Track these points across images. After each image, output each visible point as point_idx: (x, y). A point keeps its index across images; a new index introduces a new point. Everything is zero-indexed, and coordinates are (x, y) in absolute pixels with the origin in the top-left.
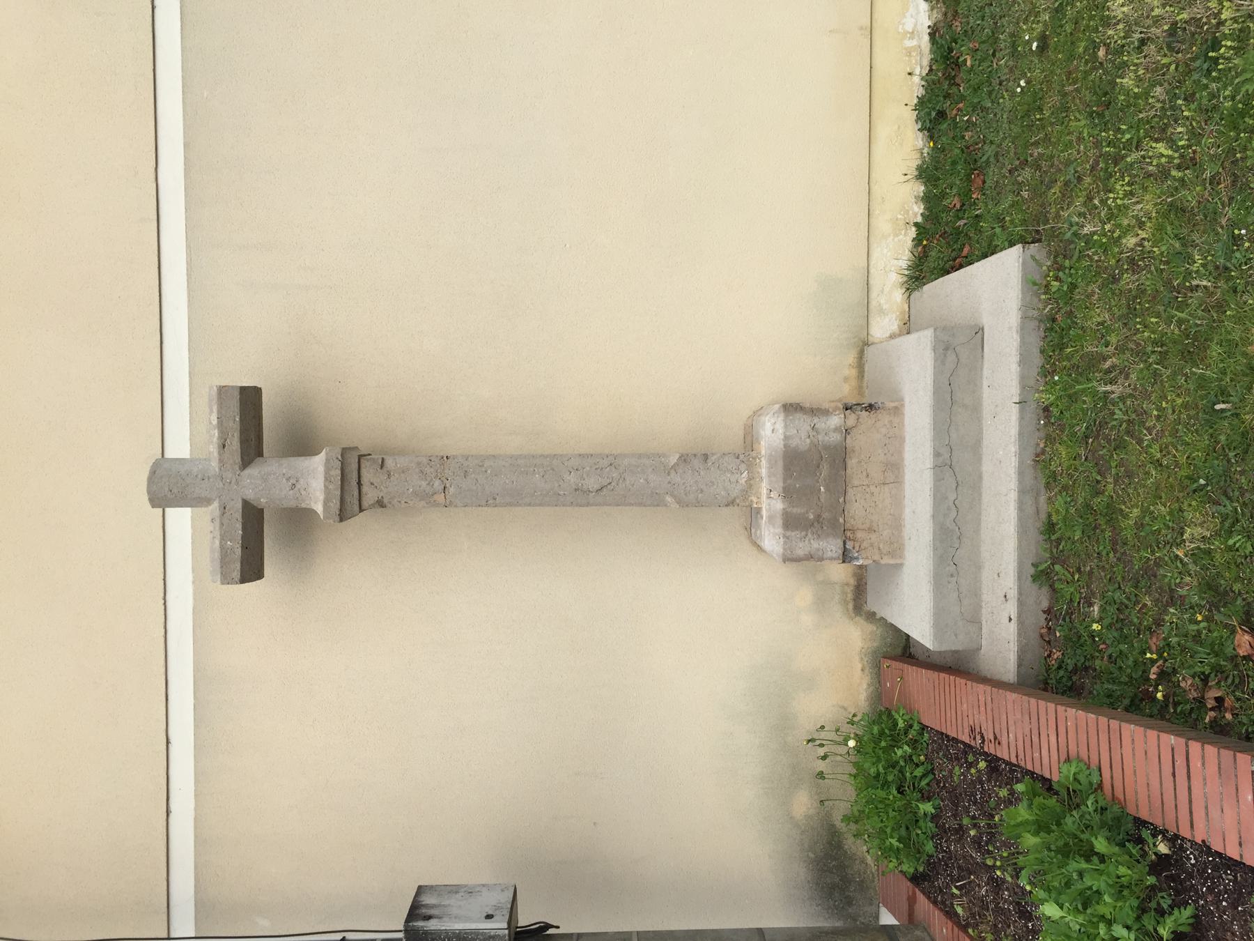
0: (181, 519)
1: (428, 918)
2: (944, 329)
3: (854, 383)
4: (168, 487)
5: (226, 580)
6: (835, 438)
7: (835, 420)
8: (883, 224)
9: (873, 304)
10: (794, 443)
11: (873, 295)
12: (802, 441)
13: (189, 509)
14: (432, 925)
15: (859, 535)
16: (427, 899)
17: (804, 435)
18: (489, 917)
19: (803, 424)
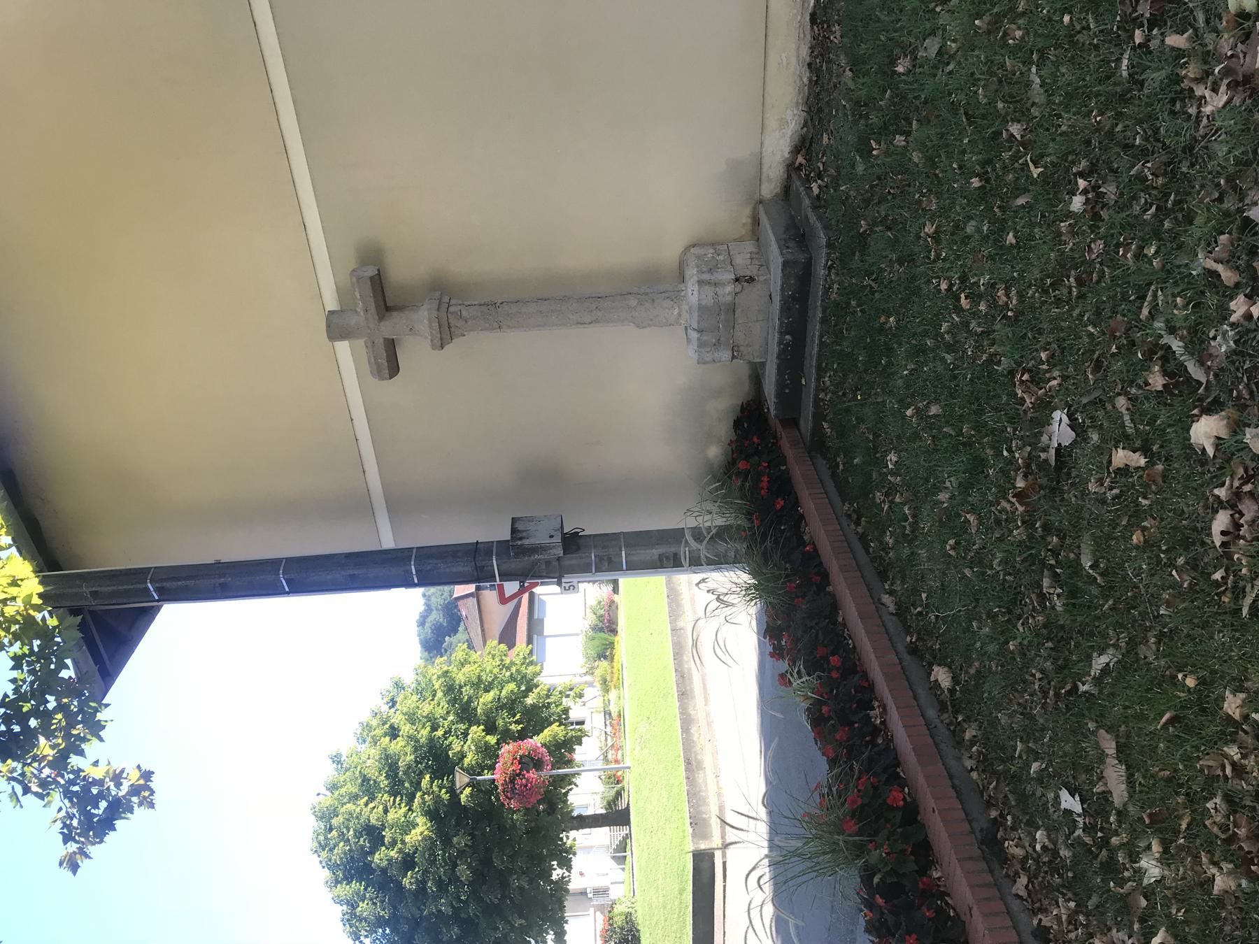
0: (343, 347)
1: (521, 539)
2: (634, 936)
3: (749, 227)
4: (337, 328)
5: (382, 378)
6: (729, 298)
7: (729, 289)
8: (772, 123)
9: (764, 175)
10: (703, 303)
11: (764, 170)
12: (709, 301)
13: (607, 828)
14: (526, 542)
15: (742, 348)
16: (520, 526)
17: (710, 298)
18: (551, 537)
19: (709, 291)
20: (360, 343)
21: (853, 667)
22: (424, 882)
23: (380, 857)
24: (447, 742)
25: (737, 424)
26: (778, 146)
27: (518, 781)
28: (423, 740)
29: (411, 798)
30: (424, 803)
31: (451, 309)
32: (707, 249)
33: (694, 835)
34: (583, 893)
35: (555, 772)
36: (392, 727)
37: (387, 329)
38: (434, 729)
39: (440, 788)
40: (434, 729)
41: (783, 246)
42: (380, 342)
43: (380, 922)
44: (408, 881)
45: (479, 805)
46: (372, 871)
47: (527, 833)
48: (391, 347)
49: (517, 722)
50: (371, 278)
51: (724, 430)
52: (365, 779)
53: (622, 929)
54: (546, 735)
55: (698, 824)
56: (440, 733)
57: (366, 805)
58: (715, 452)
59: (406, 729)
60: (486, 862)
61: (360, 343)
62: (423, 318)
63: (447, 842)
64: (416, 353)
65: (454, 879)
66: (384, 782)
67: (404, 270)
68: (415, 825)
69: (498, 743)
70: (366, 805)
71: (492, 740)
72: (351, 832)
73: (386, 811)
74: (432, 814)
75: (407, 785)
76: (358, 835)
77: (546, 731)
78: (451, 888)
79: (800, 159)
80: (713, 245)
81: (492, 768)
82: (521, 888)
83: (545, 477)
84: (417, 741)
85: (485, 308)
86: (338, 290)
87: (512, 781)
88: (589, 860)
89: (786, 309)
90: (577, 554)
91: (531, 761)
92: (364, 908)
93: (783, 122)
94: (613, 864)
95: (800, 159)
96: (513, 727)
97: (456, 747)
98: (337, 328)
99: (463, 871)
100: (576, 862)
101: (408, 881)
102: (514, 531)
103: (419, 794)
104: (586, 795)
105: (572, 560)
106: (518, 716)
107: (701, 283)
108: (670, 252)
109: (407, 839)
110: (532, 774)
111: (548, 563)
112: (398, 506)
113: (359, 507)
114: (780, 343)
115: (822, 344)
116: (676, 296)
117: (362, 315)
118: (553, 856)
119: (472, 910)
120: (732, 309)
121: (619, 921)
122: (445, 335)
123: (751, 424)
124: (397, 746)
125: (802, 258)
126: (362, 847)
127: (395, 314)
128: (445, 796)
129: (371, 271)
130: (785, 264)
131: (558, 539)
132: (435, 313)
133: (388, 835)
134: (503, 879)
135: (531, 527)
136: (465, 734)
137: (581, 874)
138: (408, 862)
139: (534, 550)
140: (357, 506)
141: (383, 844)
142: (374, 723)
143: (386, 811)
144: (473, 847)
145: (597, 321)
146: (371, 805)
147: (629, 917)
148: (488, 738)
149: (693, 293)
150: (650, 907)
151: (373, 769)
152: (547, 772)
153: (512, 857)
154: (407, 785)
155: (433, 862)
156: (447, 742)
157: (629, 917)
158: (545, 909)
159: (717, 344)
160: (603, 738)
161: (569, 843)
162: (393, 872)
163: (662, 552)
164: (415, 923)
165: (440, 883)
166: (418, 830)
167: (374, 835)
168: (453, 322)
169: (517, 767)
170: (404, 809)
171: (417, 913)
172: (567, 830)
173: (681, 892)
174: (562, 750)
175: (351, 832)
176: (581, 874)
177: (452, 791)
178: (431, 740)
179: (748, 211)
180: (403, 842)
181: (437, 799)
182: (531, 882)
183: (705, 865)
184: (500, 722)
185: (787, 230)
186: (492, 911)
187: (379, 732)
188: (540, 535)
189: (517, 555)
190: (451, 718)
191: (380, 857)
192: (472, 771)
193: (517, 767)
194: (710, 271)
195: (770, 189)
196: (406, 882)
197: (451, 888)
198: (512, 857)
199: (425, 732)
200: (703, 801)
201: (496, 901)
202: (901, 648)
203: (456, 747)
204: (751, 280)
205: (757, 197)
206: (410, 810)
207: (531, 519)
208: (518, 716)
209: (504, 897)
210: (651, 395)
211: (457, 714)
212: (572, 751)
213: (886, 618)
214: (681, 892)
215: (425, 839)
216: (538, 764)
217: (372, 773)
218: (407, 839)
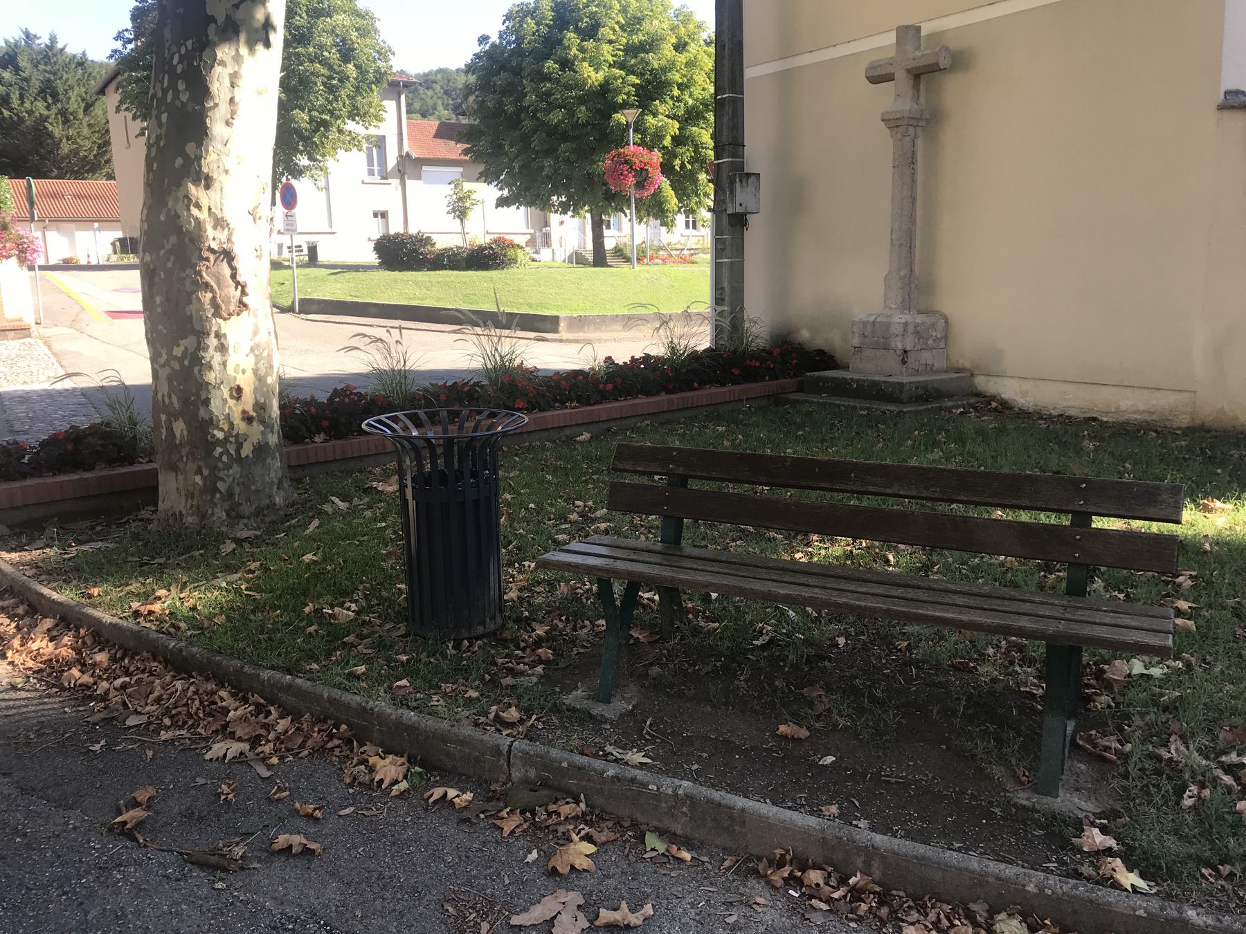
0: (891, 38)
4: (908, 33)
5: (867, 70)
8: (1026, 386)
14: (738, 185)
20: (892, 53)
21: (604, 397)
22: (550, 80)
23: (571, 37)
24: (668, 99)
25: (821, 352)
26: (1010, 390)
27: (627, 167)
28: (670, 76)
29: (622, 66)
30: (616, 79)
31: (911, 129)
32: (940, 332)
33: (571, 318)
34: (546, 224)
35: (633, 200)
36: (686, 44)
37: (901, 75)
38: (680, 86)
39: (628, 94)
40: (680, 86)
41: (918, 385)
42: (890, 70)
43: (519, 40)
44: (551, 65)
45: (612, 131)
46: (561, 30)
47: (589, 174)
48: (889, 78)
49: (683, 166)
50: (937, 64)
51: (819, 342)
52: (639, 20)
53: (505, 255)
54: (669, 192)
55: (579, 322)
56: (676, 92)
57: (618, 23)
58: (805, 335)
59: (682, 58)
60: (565, 137)
61: (892, 53)
62: (905, 105)
63: (581, 100)
64: (887, 98)
65: (551, 107)
66: (636, 39)
67: (952, 88)
68: (597, 70)
69: (664, 148)
70: (618, 23)
71: (667, 142)
72: (595, 9)
73: (611, 42)
74: (605, 87)
75: (633, 61)
76: (592, 16)
77: (672, 193)
78: (544, 105)
79: (994, 404)
80: (946, 337)
81: (643, 144)
82: (542, 168)
83: (795, 200)
84: (670, 70)
85: (909, 155)
86: (942, 32)
87: (626, 162)
88: (570, 230)
89: (875, 384)
90: (731, 227)
91: (643, 179)
92: (530, 24)
93: (1025, 394)
94: (569, 251)
95: (994, 404)
96: (677, 162)
97: (662, 108)
98: (908, 33)
99: (557, 116)
100: (567, 217)
101: (551, 65)
102: (749, 175)
103: (623, 73)
104: (625, 229)
105: (725, 220)
106: (689, 167)
107: (906, 324)
108: (948, 304)
109: (586, 64)
110: (631, 181)
111: (724, 201)
112: (785, 79)
113: (787, 49)
114: (852, 379)
115: (839, 406)
116: (906, 305)
117: (923, 55)
118: (570, 197)
119: (527, 124)
120: (886, 348)
121: (511, 253)
122: (892, 122)
123: (824, 359)
124: (667, 51)
125: (905, 396)
126: (581, 20)
127: (912, 82)
128: (620, 99)
129: (943, 63)
130: (901, 385)
131: (739, 210)
132: (906, 115)
133: (590, 44)
134: (550, 152)
135: (751, 189)
136: (673, 117)
137: (562, 223)
138: (566, 64)
139: (732, 191)
140: (787, 47)
141: (583, 40)
142: (691, 26)
143: (611, 42)
144: (575, 126)
145: (892, 245)
146: (617, 27)
147: (514, 261)
148: (668, 138)
149: (899, 318)
150: (521, 279)
151: (654, 26)
152: (632, 193)
153: (567, 161)
154: (633, 61)
155: (568, 87)
156: (668, 99)
157: (514, 261)
158: (527, 189)
159: (864, 336)
160: (678, 246)
161: (582, 212)
162: (559, 51)
163: (728, 286)
164: (517, 72)
165: (549, 94)
166: (593, 74)
167: (590, 33)
168: (901, 129)
169: (638, 166)
170: (611, 59)
171: (525, 73)
172: (591, 211)
173: (530, 306)
174: (655, 209)
175: (595, 9)
176: (562, 223)
177: (625, 105)
178: (669, 84)
179: (967, 365)
180: (584, 60)
181: (617, 92)
182: (549, 178)
183: (548, 326)
184: (680, 150)
185: (937, 390)
186: (525, 139)
187: (683, 31)
188: (743, 198)
189: (730, 177)
190: (690, 102)
191: (571, 37)
192: (639, 127)
193: (638, 166)
194: (917, 333)
195: (981, 382)
196: (550, 63)
197: (544, 105)
198: (567, 161)
199: (677, 77)
200: (598, 329)
201: (533, 146)
202: (612, 424)
203: (662, 108)
204: (904, 362)
205: (976, 372)
206: (610, 65)
207: (758, 188)
208: (689, 167)
209: (537, 153)
210: (839, 288)
211: (693, 107)
212: (656, 217)
213: (634, 420)
214: (530, 306)
215: (585, 80)
216: (640, 185)
217: (646, 26)
218: (586, 64)
